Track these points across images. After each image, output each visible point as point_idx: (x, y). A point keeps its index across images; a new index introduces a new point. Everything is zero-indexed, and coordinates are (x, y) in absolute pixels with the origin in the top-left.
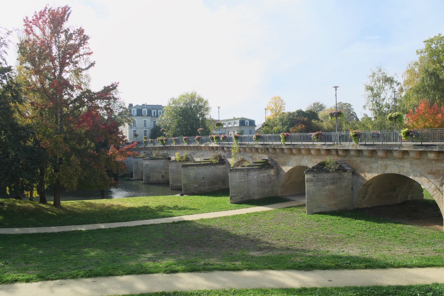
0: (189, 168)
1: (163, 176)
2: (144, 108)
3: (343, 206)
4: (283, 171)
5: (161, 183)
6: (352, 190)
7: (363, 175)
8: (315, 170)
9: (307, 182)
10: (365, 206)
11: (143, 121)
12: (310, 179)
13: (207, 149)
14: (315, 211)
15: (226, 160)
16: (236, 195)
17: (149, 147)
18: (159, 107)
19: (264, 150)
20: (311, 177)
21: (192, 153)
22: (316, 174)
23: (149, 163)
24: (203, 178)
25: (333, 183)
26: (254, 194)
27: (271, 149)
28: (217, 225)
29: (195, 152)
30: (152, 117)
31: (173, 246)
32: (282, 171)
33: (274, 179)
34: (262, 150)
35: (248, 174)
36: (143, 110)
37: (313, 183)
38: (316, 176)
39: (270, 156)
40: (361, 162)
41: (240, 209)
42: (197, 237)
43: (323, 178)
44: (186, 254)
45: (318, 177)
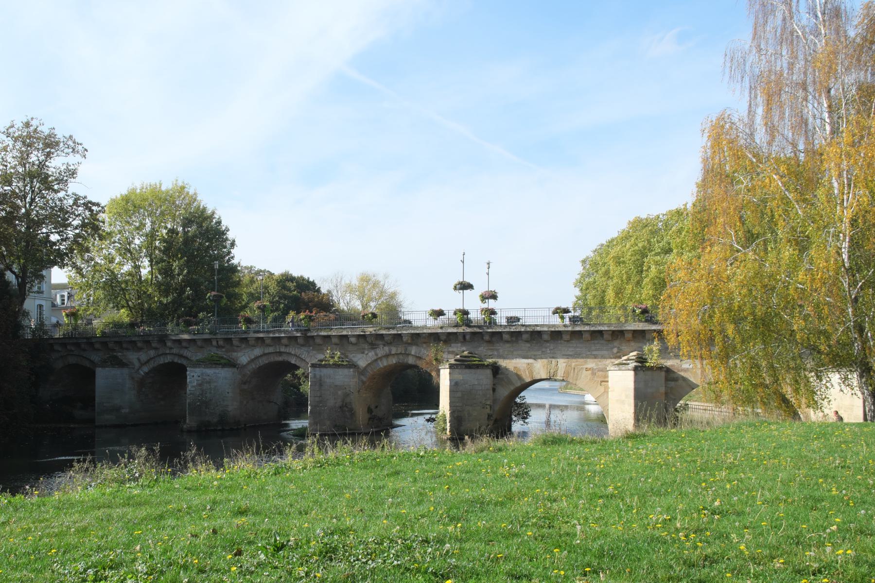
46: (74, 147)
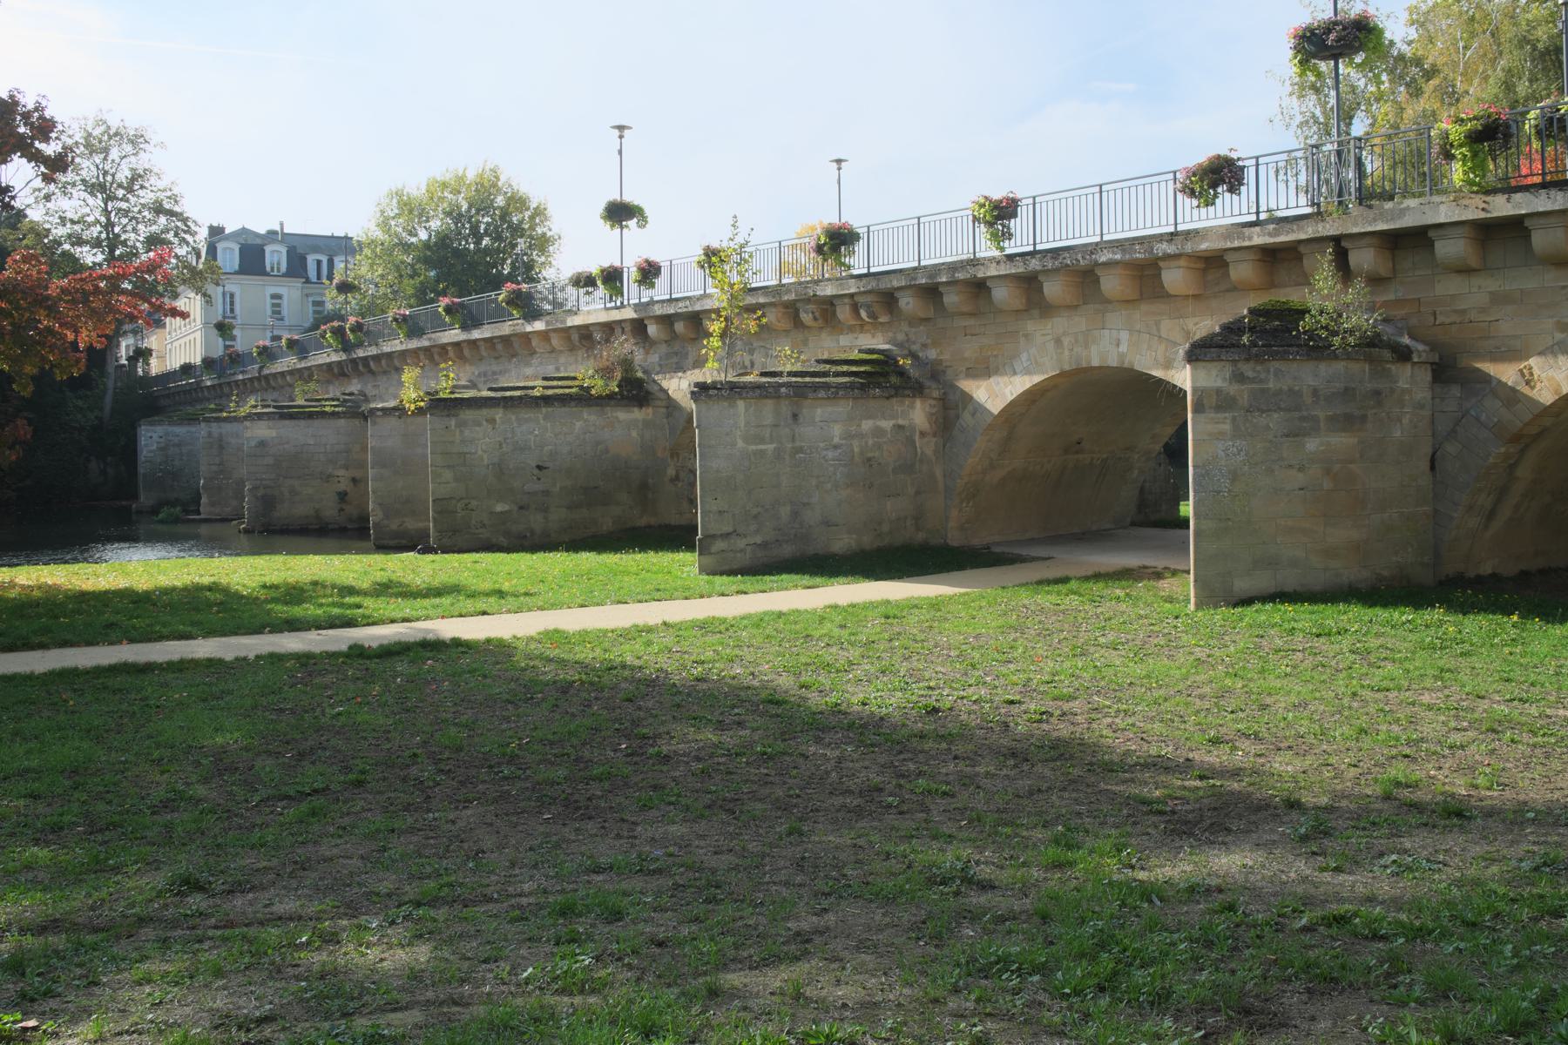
0: (468, 414)
1: (343, 496)
2: (275, 241)
3: (1394, 559)
4: (979, 409)
5: (330, 527)
6: (1433, 468)
7: (1507, 373)
8: (1245, 339)
9: (1198, 409)
10: (1486, 569)
11: (268, 298)
12: (1218, 391)
13: (556, 341)
14: (1242, 585)
15: (656, 388)
16: (730, 529)
17: (279, 370)
18: (344, 246)
19: (868, 307)
20: (1219, 383)
21: (479, 375)
22: (1251, 364)
23: (274, 435)
24: (539, 467)
25: (1347, 422)
26: (827, 523)
27: (909, 292)
28: (664, 662)
29: (495, 368)
30: (308, 281)
31: (313, 813)
32: (970, 407)
33: (929, 451)
34: (855, 309)
35: (795, 416)
36: (268, 249)
37: (1234, 419)
38: (1250, 374)
39: (901, 337)
40: (1498, 299)
41: (771, 590)
42: (539, 734)
43: (1290, 390)
44: (433, 902)
45: (1261, 381)
46: (138, 141)
